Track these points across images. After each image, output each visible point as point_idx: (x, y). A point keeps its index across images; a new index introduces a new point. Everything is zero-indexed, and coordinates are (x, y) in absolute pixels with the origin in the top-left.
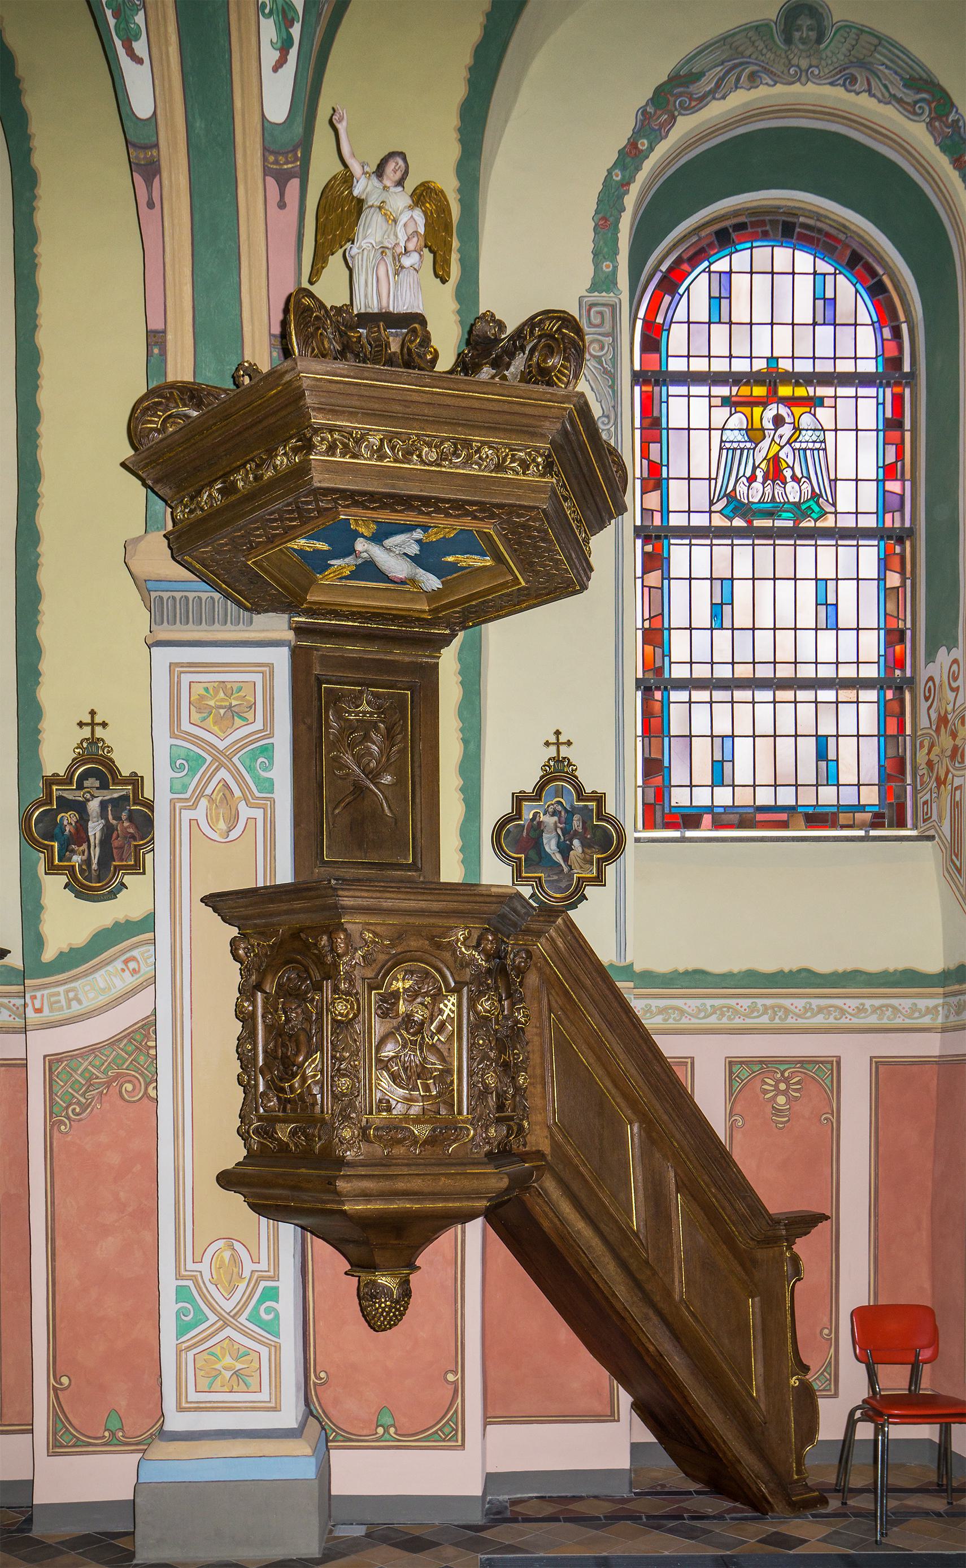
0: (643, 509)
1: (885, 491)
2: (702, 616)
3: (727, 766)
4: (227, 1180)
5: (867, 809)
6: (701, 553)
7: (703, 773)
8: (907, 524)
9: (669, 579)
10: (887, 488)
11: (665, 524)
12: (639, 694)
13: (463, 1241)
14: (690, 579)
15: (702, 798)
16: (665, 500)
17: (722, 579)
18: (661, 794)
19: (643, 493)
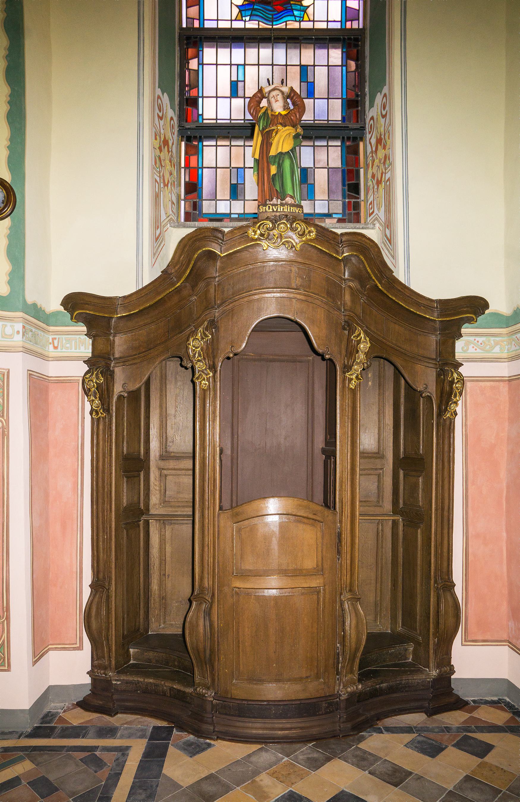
0: (187, 18)
1: (346, 7)
2: (225, 89)
3: (240, 85)
4: (88, 673)
5: (334, 216)
6: (224, 54)
7: (224, 192)
8: (361, 27)
9: (203, 64)
10: (348, 5)
11: (202, 26)
12: (183, 144)
13: (8, 494)
14: (217, 65)
15: (223, 208)
16: (201, 12)
17: (238, 65)
18: (196, 206)
19: (187, 7)
